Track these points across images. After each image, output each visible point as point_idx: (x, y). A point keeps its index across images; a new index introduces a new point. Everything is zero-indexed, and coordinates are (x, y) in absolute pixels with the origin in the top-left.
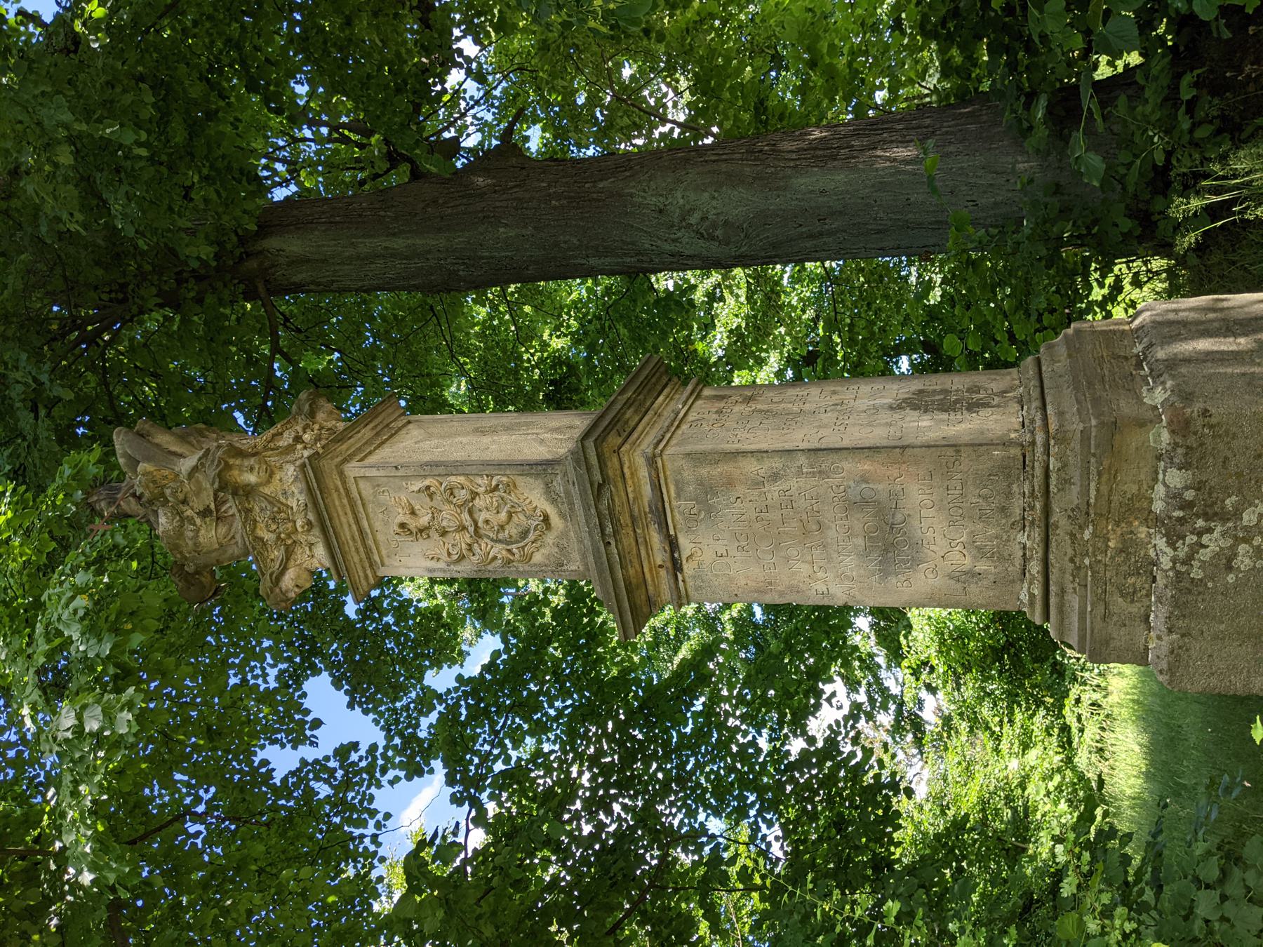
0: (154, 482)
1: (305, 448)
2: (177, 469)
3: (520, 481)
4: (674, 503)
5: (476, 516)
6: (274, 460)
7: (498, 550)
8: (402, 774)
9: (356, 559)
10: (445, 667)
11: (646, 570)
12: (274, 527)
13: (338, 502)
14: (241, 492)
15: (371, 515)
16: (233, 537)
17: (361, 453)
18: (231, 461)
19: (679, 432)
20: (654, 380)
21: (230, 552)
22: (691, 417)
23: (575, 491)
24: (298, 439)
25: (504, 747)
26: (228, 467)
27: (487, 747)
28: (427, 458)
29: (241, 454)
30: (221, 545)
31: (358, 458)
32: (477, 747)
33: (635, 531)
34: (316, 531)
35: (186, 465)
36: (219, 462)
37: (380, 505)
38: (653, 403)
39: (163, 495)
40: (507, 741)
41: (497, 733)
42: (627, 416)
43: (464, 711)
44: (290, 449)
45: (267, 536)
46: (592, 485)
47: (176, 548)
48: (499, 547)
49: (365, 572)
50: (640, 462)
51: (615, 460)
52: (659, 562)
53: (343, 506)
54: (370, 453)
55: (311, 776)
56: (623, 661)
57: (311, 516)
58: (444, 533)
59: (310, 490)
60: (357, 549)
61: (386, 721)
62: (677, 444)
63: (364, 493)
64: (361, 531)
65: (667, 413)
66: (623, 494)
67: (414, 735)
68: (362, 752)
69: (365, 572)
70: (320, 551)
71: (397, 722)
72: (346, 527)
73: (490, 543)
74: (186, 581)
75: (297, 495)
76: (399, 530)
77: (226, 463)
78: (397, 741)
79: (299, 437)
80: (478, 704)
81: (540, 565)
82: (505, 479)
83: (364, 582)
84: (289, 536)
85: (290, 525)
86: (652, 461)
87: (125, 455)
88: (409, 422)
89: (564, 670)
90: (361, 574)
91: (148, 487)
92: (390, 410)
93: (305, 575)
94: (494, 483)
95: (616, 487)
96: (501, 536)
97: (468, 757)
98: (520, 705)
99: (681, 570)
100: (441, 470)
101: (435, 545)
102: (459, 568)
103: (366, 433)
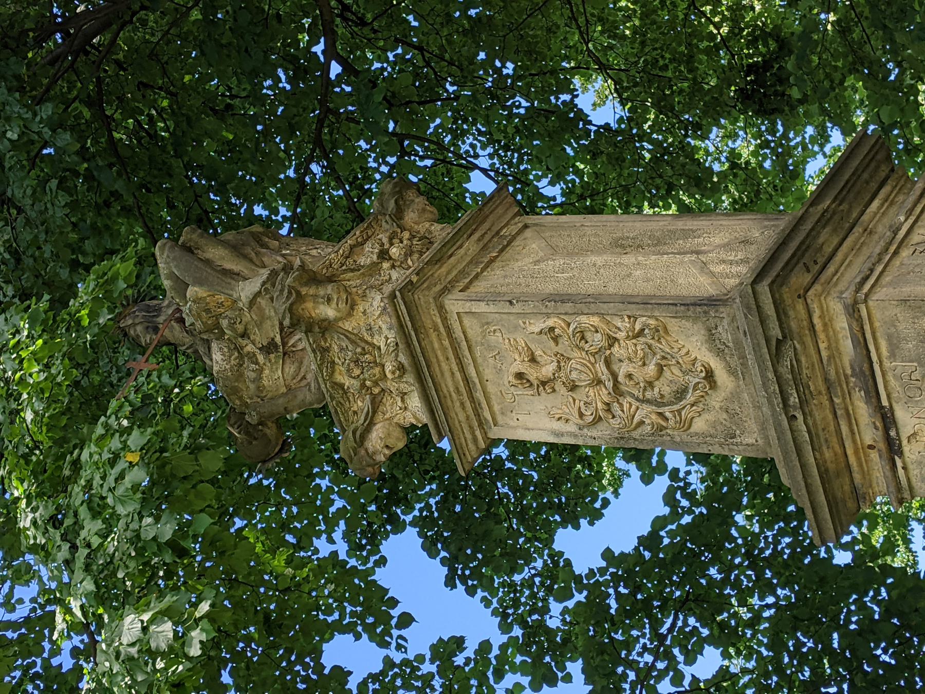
0: (208, 311)
1: (393, 267)
2: (235, 296)
3: (673, 325)
4: (887, 364)
5: (615, 367)
6: (353, 281)
7: (645, 412)
8: (525, 681)
9: (462, 416)
10: (583, 522)
11: (850, 452)
12: (357, 372)
13: (437, 344)
14: (317, 329)
15: (480, 360)
16: (304, 378)
17: (465, 281)
18: (304, 290)
19: (897, 262)
20: (865, 176)
21: (300, 397)
22: (915, 238)
23: (747, 344)
24: (384, 255)
25: (671, 658)
26: (300, 298)
27: (648, 658)
28: (550, 288)
29: (314, 279)
30: (289, 388)
31: (461, 285)
32: (634, 656)
33: (831, 401)
34: (410, 378)
35: (246, 290)
36: (290, 293)
37: (490, 348)
38: (862, 213)
39: (217, 325)
40: (676, 651)
41: (662, 638)
42: (821, 240)
43: (613, 604)
44: (374, 268)
45: (347, 382)
46: (767, 341)
47: (235, 391)
48: (646, 409)
49: (473, 434)
50: (836, 308)
51: (800, 307)
52: (868, 441)
53: (444, 349)
54: (476, 277)
55: (399, 682)
56: (855, 541)
57: (402, 358)
58: (573, 388)
59: (401, 326)
60: (462, 404)
61: (501, 601)
62: (890, 284)
63: (470, 333)
64: (466, 380)
65: (882, 229)
66: (812, 351)
67: (541, 624)
68: (470, 652)
69: (473, 434)
70: (415, 402)
71: (516, 603)
72: (447, 375)
73: (635, 404)
74: (247, 433)
75: (386, 332)
76: (515, 382)
77: (298, 293)
78: (517, 632)
79: (382, 257)
80: (633, 594)
81: (704, 435)
82: (652, 322)
83: (472, 446)
84: (376, 384)
85: (377, 370)
86: (852, 310)
87: (171, 276)
88: (526, 226)
89: (762, 551)
90: (469, 436)
91: (199, 316)
92: (500, 211)
93: (397, 433)
94: (638, 327)
95: (803, 343)
96: (649, 394)
97: (620, 670)
98: (698, 600)
99: (901, 454)
100: (568, 307)
101: (560, 400)
102: (594, 433)
103: (470, 247)
